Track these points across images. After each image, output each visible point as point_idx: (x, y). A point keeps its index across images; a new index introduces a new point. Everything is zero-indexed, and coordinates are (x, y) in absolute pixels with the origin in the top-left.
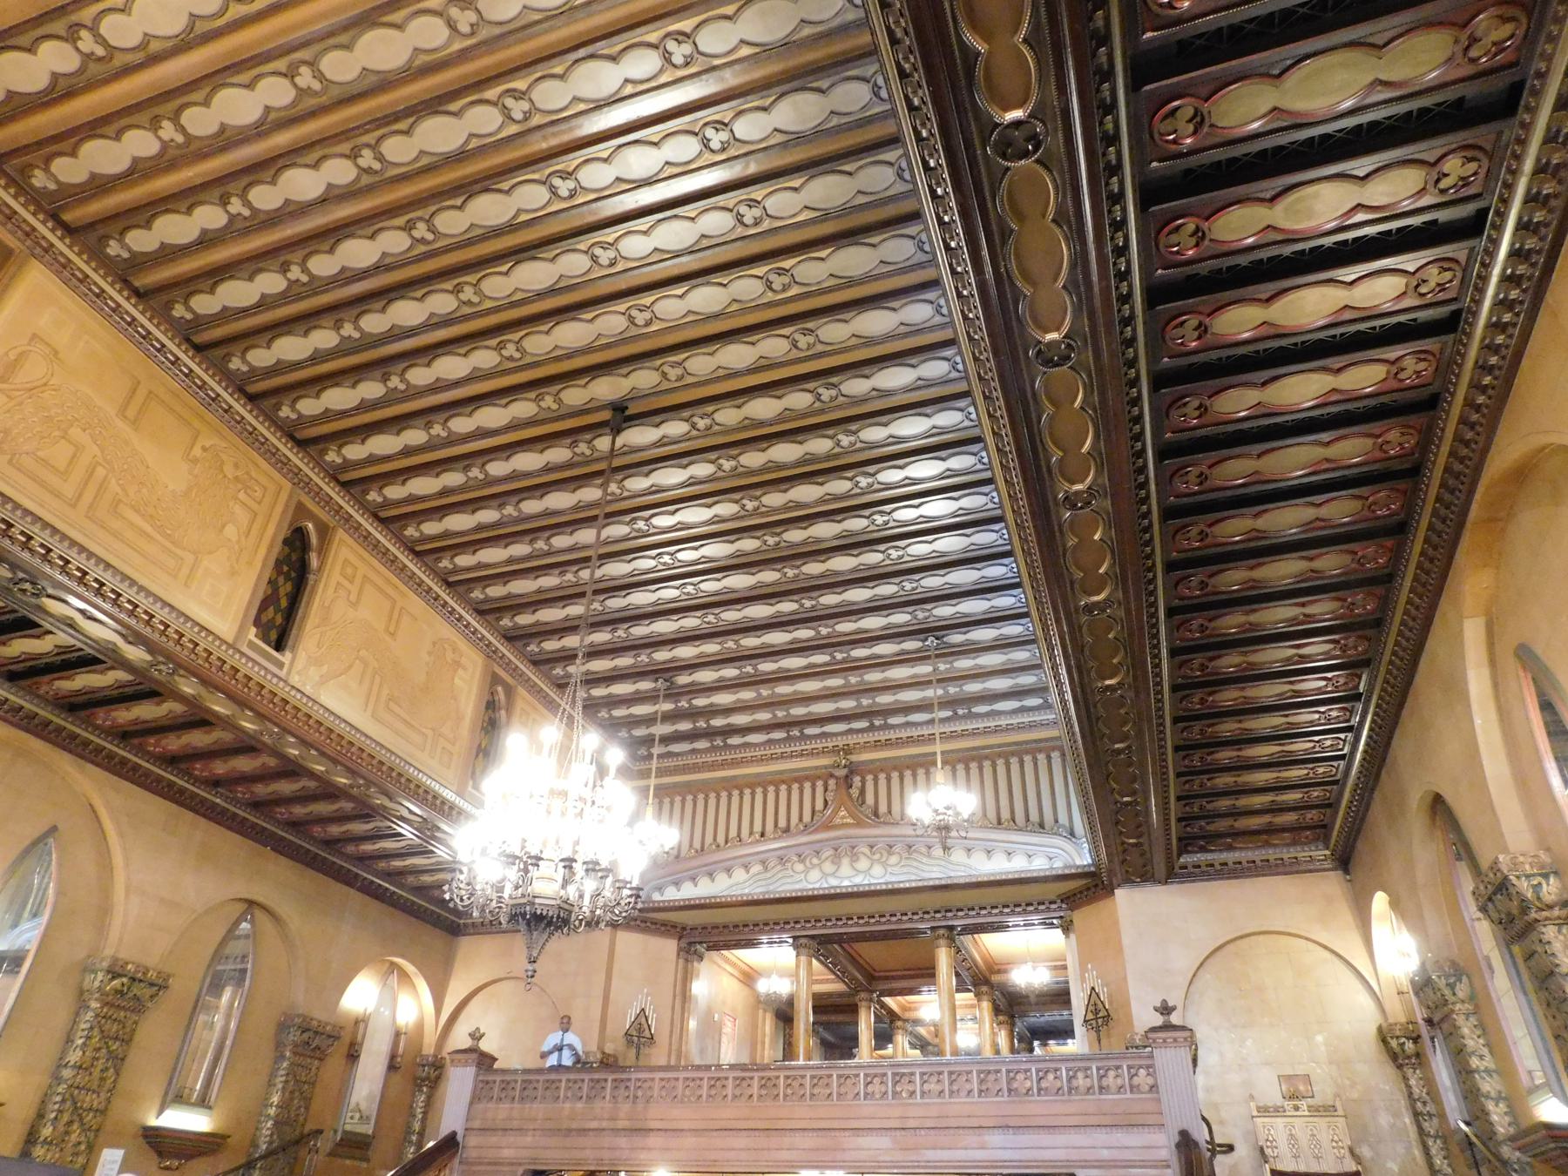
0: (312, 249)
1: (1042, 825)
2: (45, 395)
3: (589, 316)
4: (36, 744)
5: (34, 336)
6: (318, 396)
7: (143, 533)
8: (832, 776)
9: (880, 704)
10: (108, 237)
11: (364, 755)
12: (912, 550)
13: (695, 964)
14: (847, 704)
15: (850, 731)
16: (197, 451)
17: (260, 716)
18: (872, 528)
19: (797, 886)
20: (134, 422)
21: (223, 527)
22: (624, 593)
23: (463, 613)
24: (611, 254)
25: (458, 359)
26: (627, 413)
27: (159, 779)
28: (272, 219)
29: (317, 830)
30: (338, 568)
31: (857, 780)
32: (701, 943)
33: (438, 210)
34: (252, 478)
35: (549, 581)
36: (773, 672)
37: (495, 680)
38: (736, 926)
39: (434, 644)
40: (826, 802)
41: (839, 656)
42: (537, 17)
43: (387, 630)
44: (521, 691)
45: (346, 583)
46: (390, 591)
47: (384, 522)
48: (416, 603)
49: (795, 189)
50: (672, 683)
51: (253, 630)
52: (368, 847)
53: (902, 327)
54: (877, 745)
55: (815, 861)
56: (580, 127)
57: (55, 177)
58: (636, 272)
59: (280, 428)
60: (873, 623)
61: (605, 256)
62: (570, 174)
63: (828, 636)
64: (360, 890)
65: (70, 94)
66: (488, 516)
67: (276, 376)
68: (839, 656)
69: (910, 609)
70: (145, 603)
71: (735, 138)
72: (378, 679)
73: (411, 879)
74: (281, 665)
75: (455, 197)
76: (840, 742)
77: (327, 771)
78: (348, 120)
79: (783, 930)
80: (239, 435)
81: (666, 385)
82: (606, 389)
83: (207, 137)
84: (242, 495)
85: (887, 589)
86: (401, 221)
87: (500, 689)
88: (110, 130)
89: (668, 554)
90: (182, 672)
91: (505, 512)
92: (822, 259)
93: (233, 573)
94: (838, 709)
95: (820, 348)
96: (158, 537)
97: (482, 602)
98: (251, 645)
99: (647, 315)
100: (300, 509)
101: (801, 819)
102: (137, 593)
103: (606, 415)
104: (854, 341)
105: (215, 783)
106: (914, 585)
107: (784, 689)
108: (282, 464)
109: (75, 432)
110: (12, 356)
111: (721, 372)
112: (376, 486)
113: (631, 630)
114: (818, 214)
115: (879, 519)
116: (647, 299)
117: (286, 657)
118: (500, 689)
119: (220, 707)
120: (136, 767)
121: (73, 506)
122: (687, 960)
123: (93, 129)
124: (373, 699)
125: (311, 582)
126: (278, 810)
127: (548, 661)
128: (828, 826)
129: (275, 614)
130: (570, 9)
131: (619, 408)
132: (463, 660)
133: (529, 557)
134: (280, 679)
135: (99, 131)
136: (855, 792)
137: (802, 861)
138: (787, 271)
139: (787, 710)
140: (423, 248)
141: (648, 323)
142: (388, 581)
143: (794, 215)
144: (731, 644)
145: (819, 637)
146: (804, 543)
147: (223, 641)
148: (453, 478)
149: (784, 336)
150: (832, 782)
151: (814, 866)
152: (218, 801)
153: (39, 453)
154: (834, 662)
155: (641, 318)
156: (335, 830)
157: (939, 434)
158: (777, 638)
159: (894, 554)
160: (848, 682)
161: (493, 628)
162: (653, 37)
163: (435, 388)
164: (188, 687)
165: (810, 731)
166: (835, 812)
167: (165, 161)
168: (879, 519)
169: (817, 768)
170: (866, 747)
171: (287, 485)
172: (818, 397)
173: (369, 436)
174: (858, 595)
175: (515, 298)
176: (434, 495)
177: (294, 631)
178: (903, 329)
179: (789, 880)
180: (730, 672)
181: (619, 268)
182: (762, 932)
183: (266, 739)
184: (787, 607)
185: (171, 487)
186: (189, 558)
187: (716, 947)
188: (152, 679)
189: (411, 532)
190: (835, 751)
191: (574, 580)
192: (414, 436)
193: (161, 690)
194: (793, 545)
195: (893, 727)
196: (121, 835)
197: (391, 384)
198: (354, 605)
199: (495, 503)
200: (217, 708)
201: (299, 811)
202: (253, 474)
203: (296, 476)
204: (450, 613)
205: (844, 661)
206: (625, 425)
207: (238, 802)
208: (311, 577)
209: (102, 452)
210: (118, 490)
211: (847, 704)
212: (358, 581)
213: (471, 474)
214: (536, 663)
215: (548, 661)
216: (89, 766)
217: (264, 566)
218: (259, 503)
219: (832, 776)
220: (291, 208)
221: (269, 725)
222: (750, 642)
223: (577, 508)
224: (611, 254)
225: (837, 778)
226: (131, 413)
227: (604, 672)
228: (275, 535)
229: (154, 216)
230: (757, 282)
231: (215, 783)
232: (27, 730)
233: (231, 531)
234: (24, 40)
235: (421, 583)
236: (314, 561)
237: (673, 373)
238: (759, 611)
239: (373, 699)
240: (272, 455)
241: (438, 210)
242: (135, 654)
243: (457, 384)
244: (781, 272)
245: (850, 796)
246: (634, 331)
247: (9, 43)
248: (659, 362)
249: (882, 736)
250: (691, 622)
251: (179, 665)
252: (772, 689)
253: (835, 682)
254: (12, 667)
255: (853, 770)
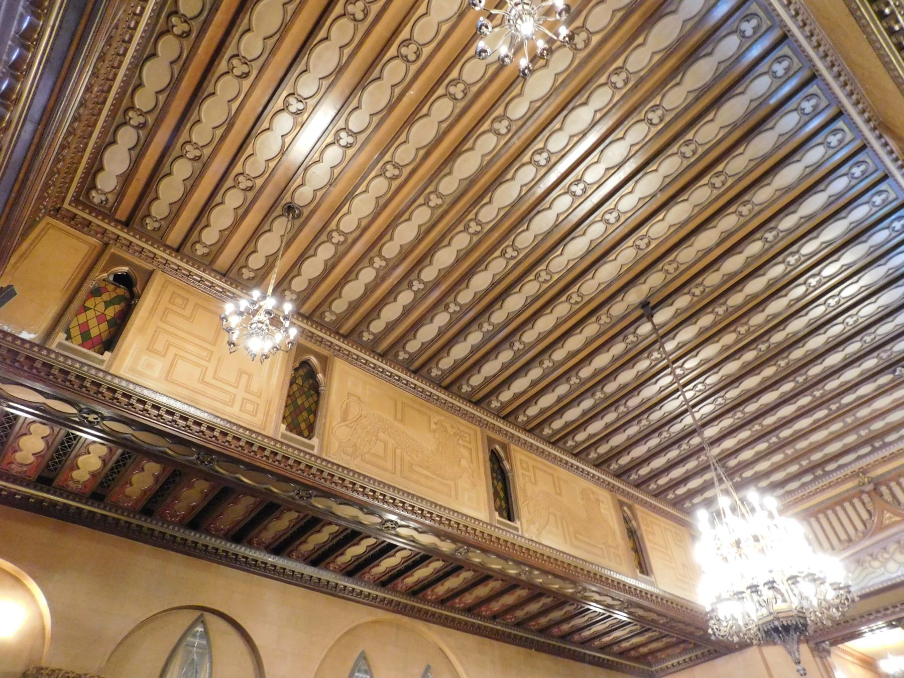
0: (457, 290)
1: (850, 540)
2: (363, 420)
3: (613, 257)
4: (405, 619)
5: (349, 394)
6: (479, 372)
7: (427, 477)
8: (862, 492)
9: (875, 431)
10: (362, 332)
11: (579, 570)
12: (862, 313)
13: (828, 658)
14: (851, 439)
15: (860, 458)
16: (433, 426)
17: (518, 563)
18: (829, 309)
19: (883, 578)
20: (402, 421)
21: (460, 461)
22: (679, 420)
23: (589, 469)
24: (615, 214)
25: (547, 316)
26: (651, 305)
27: (466, 623)
28: (436, 284)
29: (555, 631)
30: (519, 466)
31: (883, 489)
32: (824, 642)
33: (515, 237)
34: (461, 431)
35: (633, 430)
36: (792, 435)
37: (621, 504)
38: (862, 617)
39: (582, 493)
40: (869, 512)
41: (834, 407)
42: (538, 104)
43: (556, 493)
44: (637, 507)
45: (527, 473)
46: (550, 471)
47: (530, 431)
48: (563, 472)
49: (712, 120)
50: (726, 468)
51: (497, 514)
52: (586, 633)
53: (723, 234)
54: (885, 460)
55: (886, 556)
56: (534, 193)
57: (334, 312)
58: (604, 241)
59: (464, 399)
60: (851, 374)
61: (611, 218)
62: (580, 180)
63: (822, 396)
64: (590, 663)
65: (334, 267)
66: (587, 404)
67: (456, 370)
68: (834, 407)
69: (875, 354)
70: (445, 515)
71: (666, 111)
72: (564, 523)
73: (615, 648)
74: (516, 529)
75: (654, 98)
76: (855, 467)
77: (560, 587)
78: (448, 223)
79: (877, 619)
80: (447, 410)
81: (669, 277)
82: (635, 296)
83: (395, 257)
84: (461, 441)
85: (853, 347)
86: (498, 253)
87: (625, 508)
88: (353, 276)
89: (700, 383)
90: (472, 549)
91: (597, 397)
92: (741, 154)
93: (474, 485)
94: (844, 445)
95: (757, 209)
96: (435, 477)
97: (597, 459)
98: (499, 522)
99: (646, 240)
100: (490, 441)
101: (856, 529)
102: (440, 510)
103: (639, 312)
104: (778, 193)
105: (494, 617)
106: (873, 336)
107: (802, 445)
108: (472, 418)
109: (381, 435)
110: (344, 406)
111: (700, 254)
112: (521, 412)
113: (691, 442)
114: (730, 127)
115: (832, 302)
116: (643, 231)
117: (517, 524)
118: (625, 508)
119: (496, 565)
120: (454, 619)
121: (394, 473)
122: (821, 658)
123: (346, 279)
124: (567, 536)
125: (510, 478)
126: (531, 624)
127: (644, 482)
128: (882, 528)
129: (501, 502)
130: (555, 89)
131: (644, 305)
132: (600, 498)
133: (617, 420)
134: (518, 536)
135: (348, 279)
136: (889, 498)
137: (876, 559)
138: (722, 172)
139: (809, 458)
140: (513, 262)
141: (648, 244)
142: (545, 465)
143: (717, 135)
144: (757, 427)
145: (815, 399)
146: (786, 339)
147: (484, 523)
148: (562, 389)
149: (732, 213)
150: (865, 497)
151: (887, 560)
152: (499, 627)
153: (371, 451)
154: (831, 412)
155: (642, 244)
156: (566, 627)
157: (826, 247)
158: (787, 411)
159: (850, 321)
160: (845, 423)
161: (607, 473)
162: (603, 79)
163: (539, 340)
164: (477, 558)
165: (830, 467)
166: (881, 516)
167: (380, 280)
168: (832, 302)
169: (847, 491)
170: (877, 464)
171: (478, 429)
172: (766, 240)
173: (510, 384)
174: (834, 359)
175: (569, 267)
176: (554, 404)
177: (515, 508)
178: (808, 170)
179: (873, 576)
180: (762, 446)
181: (622, 220)
182: (863, 624)
183: (523, 577)
184: (787, 387)
185: (430, 449)
186: (452, 483)
187: (835, 642)
188: (456, 560)
189: (547, 431)
190: (855, 475)
191: (648, 423)
192: (535, 373)
193: (463, 565)
194: (779, 344)
195: (891, 443)
196: (461, 662)
197: (515, 348)
198: (535, 483)
199: (589, 394)
200: (493, 566)
201: (543, 621)
202: (461, 428)
203: (480, 422)
204: (582, 472)
205: (838, 409)
206: (653, 312)
207: (509, 625)
208: (509, 474)
209: (395, 440)
210: (409, 458)
211: (851, 439)
212: (531, 469)
213: (572, 382)
214: (638, 485)
215: (644, 482)
216: (431, 625)
217: (486, 476)
218: (470, 443)
219: (862, 492)
220: (442, 273)
221: (523, 567)
222: (769, 420)
223: (637, 377)
224: (615, 214)
225: (868, 493)
226: (399, 417)
227: (680, 476)
228: (484, 458)
229: (380, 311)
230: (706, 188)
231: (494, 617)
232: (398, 613)
233: (464, 462)
234: (311, 252)
235: (561, 460)
236: (507, 466)
237: (671, 268)
238: (769, 398)
239: (567, 536)
240: (465, 415)
241: (515, 237)
242: (446, 547)
243: (550, 332)
244: (718, 174)
245: (886, 502)
246: (641, 254)
247: (306, 257)
248: (660, 266)
249: (886, 452)
250: (727, 422)
251: (470, 545)
252: (794, 447)
253: (837, 427)
254: (382, 579)
255: (877, 483)
